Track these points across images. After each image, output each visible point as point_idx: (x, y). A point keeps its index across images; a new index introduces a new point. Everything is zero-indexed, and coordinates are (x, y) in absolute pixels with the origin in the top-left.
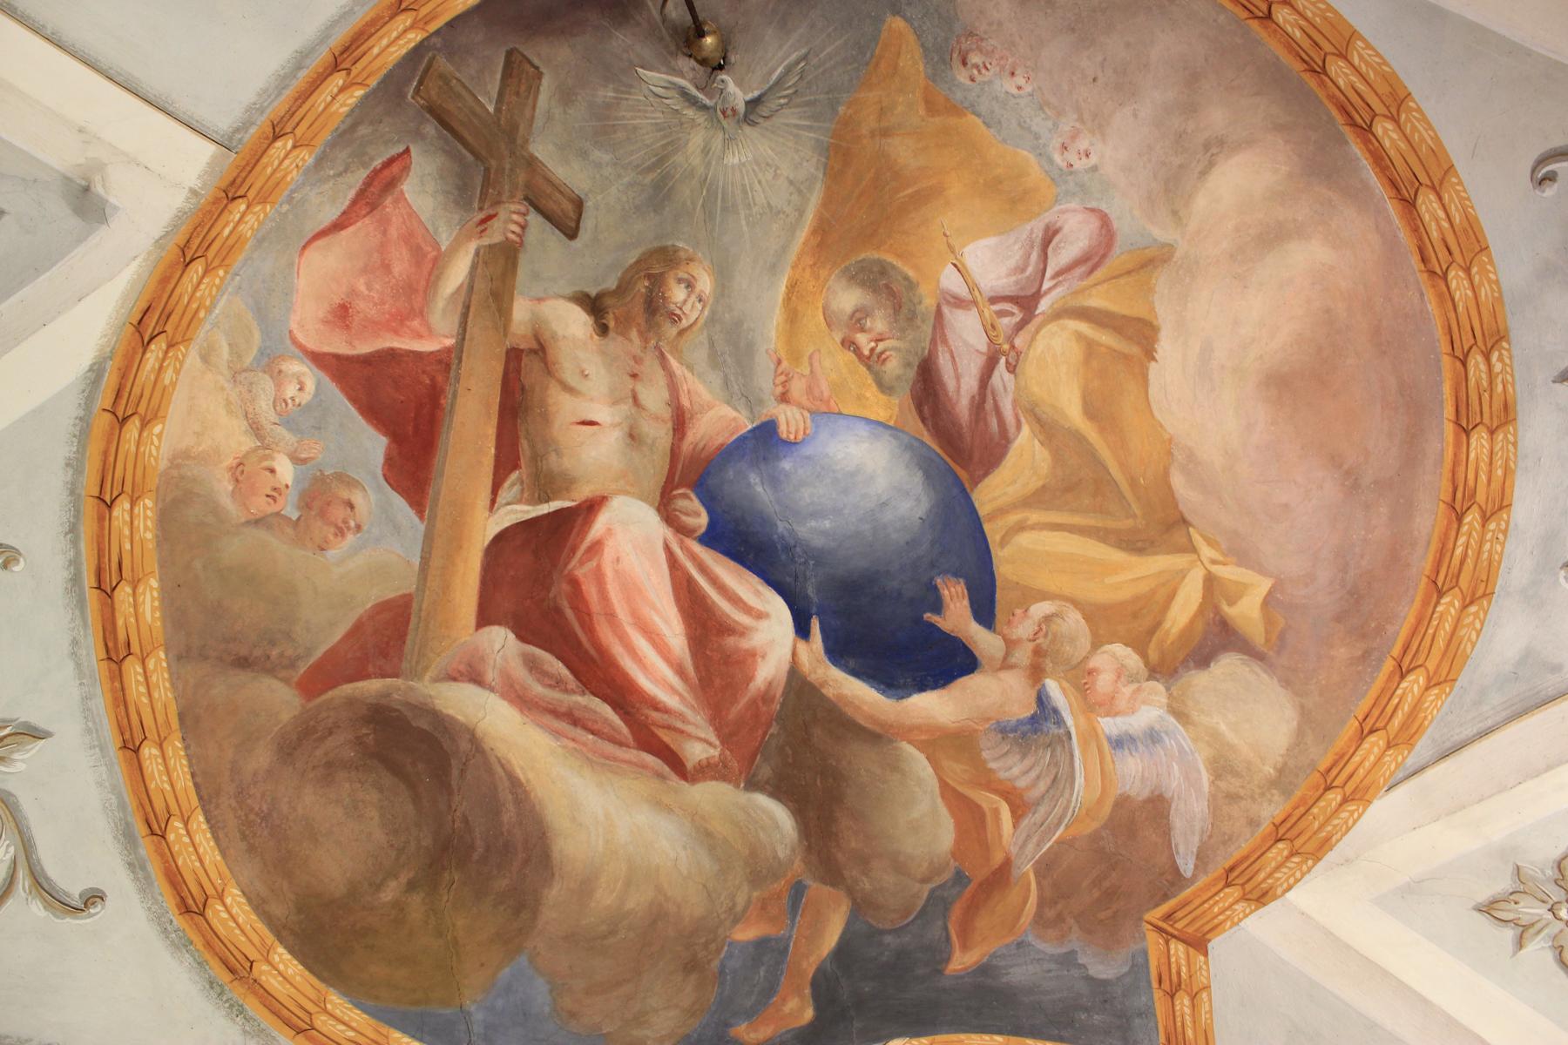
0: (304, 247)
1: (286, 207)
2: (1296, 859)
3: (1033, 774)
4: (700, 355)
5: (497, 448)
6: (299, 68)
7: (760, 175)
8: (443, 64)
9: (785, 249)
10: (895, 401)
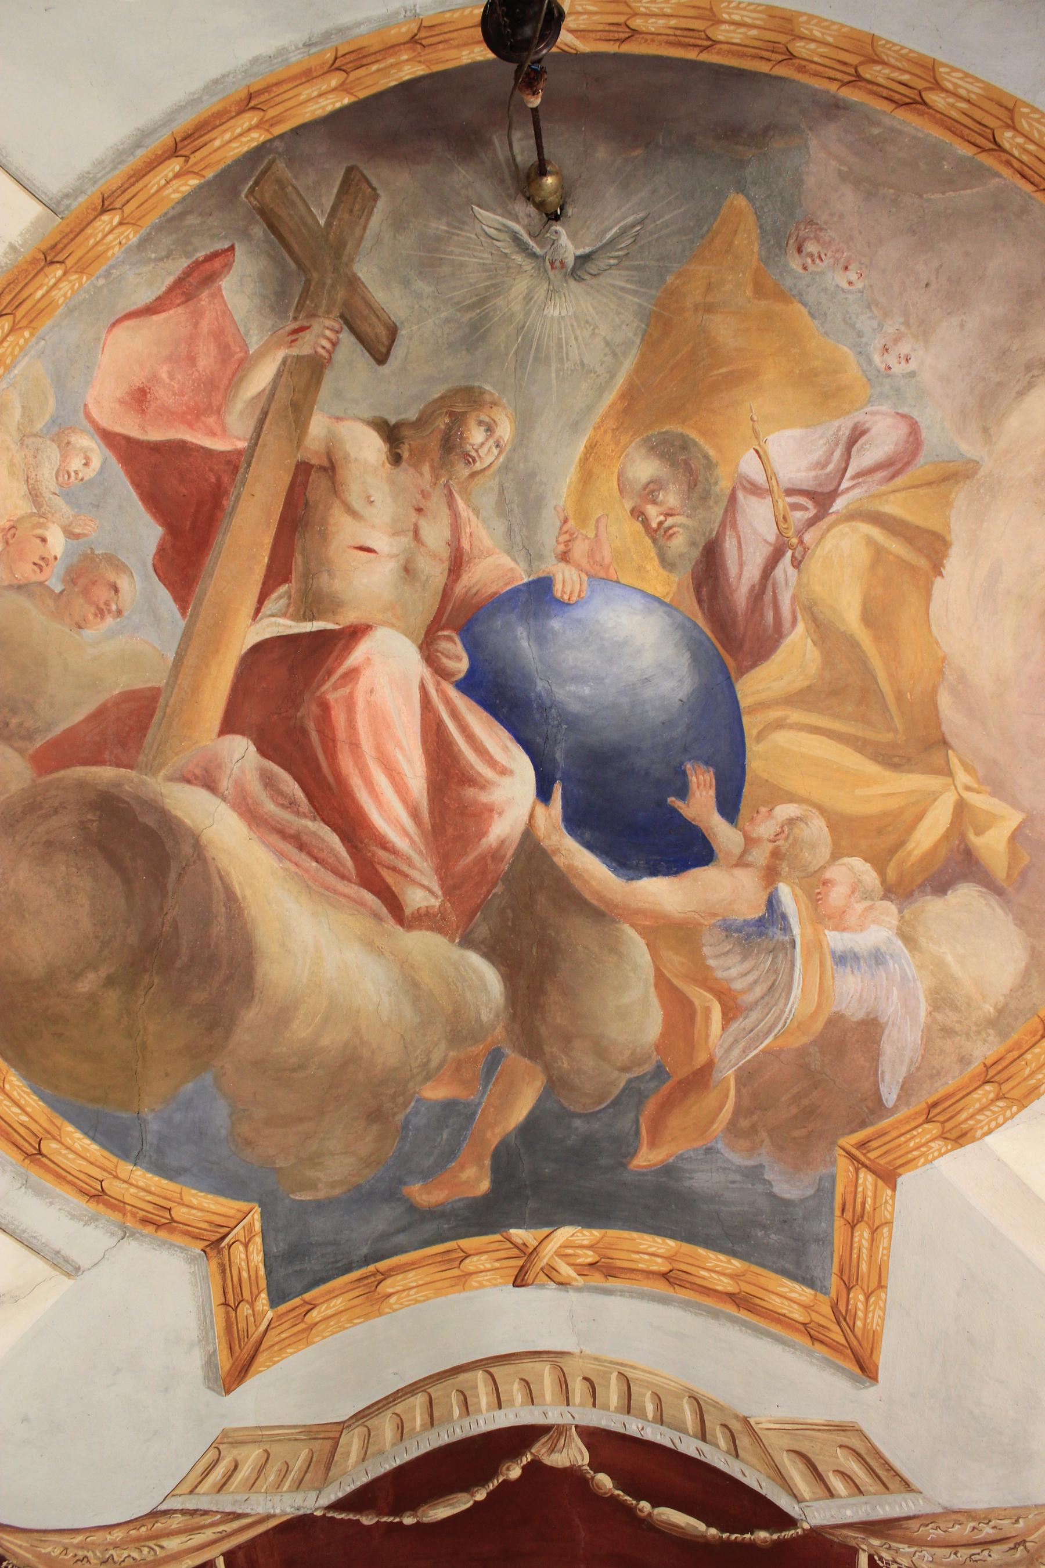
0: (114, 325)
1: (102, 282)
2: (1001, 1104)
3: (751, 978)
4: (488, 501)
5: (270, 558)
6: (138, 146)
7: (578, 332)
8: (281, 167)
9: (589, 409)
10: (675, 578)
